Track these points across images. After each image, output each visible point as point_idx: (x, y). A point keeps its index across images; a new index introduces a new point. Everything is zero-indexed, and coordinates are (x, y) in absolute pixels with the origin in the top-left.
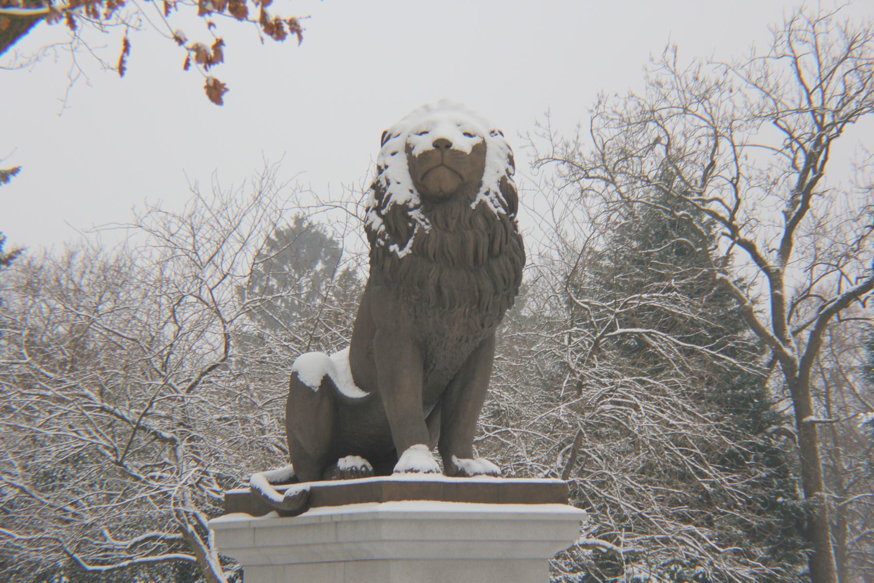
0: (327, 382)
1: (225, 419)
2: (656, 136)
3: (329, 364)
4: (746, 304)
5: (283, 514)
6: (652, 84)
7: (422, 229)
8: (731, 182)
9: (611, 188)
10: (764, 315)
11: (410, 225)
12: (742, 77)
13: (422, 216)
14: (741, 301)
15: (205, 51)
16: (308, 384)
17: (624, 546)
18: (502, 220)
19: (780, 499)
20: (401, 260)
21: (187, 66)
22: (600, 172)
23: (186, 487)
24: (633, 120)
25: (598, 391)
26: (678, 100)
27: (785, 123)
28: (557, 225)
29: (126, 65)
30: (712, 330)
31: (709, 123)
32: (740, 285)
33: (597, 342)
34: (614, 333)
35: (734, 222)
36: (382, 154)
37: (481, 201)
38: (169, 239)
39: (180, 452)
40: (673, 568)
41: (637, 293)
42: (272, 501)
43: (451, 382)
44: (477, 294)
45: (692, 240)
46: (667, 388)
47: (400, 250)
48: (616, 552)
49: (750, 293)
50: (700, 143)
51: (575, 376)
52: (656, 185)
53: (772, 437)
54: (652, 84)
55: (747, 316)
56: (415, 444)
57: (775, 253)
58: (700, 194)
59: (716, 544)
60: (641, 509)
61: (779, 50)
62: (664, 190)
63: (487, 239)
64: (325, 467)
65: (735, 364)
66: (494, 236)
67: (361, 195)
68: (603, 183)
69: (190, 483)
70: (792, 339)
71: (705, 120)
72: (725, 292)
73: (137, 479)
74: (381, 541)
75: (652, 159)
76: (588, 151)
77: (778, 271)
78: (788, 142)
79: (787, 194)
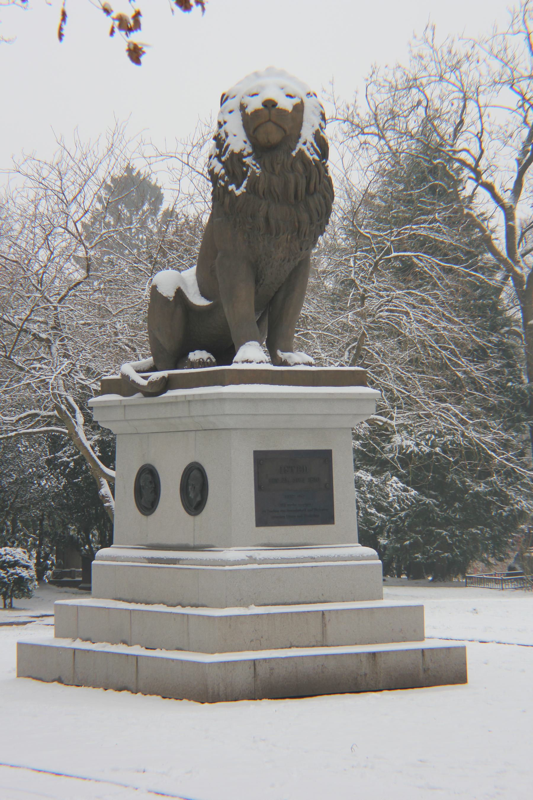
0: (179, 292)
1: (87, 324)
2: (417, 100)
3: (180, 279)
4: (487, 233)
5: (147, 395)
6: (415, 57)
7: (254, 172)
8: (477, 136)
9: (383, 142)
10: (500, 243)
11: (245, 169)
12: (485, 50)
13: (254, 162)
14: (483, 230)
15: (126, 20)
16: (165, 295)
17: (396, 420)
18: (316, 165)
19: (510, 384)
20: (237, 198)
21: (112, 33)
22: (374, 129)
23: (60, 376)
24: (399, 87)
25: (376, 302)
26: (435, 70)
27: (519, 87)
28: (353, 170)
29: (63, 32)
30: (468, 253)
31: (460, 89)
32: (481, 218)
33: (376, 263)
34: (390, 256)
35: (478, 168)
36: (222, 112)
37: (300, 149)
38: (41, 182)
39: (54, 350)
40: (427, 437)
41: (409, 224)
42: (138, 385)
43: (276, 293)
44: (297, 224)
45: (445, 183)
46: (430, 299)
47: (237, 189)
48: (390, 425)
49: (490, 224)
50: (452, 105)
51: (358, 290)
52: (418, 139)
53: (504, 336)
54: (415, 57)
55: (486, 242)
56: (249, 341)
57: (509, 192)
58: (452, 146)
59: (467, 418)
60: (409, 392)
61: (516, 27)
62: (423, 143)
63: (304, 181)
64: (179, 359)
65: (483, 279)
66: (310, 178)
67: (191, 148)
68: (376, 139)
69: (63, 373)
70: (521, 260)
71: (456, 86)
72: (473, 223)
73: (21, 369)
74: (224, 414)
75: (415, 118)
76: (364, 112)
77: (511, 206)
78: (521, 103)
79: (520, 146)
